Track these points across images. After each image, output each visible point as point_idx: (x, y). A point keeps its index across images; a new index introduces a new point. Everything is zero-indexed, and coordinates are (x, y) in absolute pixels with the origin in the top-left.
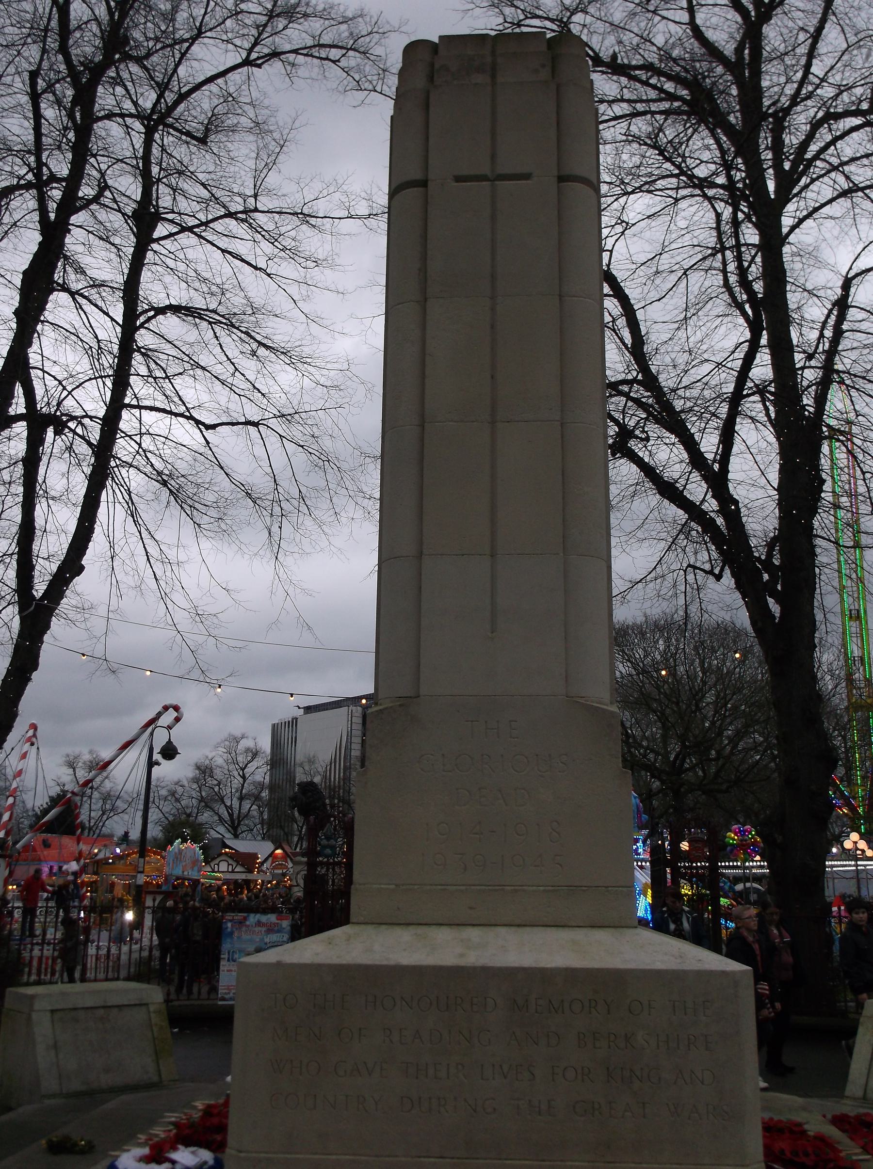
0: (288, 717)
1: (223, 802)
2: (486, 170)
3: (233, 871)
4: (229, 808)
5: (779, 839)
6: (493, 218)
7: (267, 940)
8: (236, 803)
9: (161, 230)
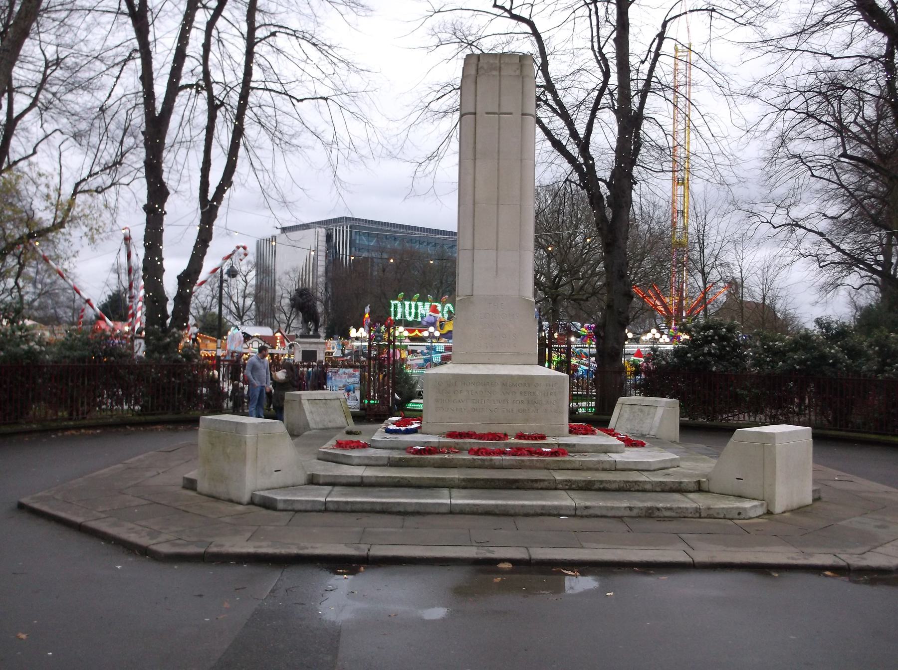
0: (268, 235)
1: (231, 298)
2: (497, 111)
5: (602, 334)
6: (499, 129)
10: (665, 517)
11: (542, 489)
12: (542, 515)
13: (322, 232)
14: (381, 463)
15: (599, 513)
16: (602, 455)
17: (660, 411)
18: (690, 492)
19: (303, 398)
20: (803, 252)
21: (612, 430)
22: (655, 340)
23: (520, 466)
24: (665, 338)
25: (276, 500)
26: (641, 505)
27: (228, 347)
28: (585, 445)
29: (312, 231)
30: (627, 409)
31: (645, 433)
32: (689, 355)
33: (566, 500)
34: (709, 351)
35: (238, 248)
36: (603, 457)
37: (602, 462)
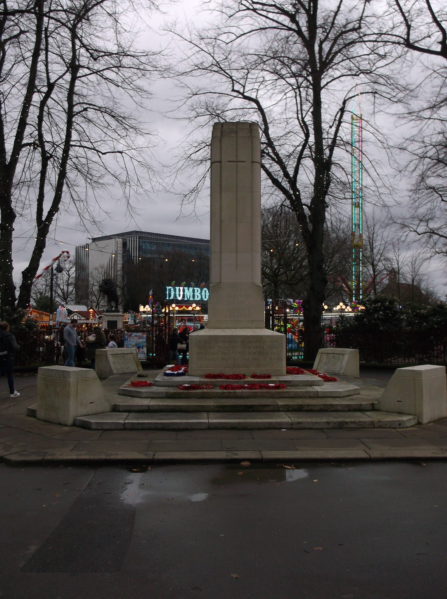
0: (83, 243)
2: (235, 160)
3: (80, 319)
4: (62, 290)
5: (307, 307)
7: (139, 341)
8: (65, 288)
9: (81, 72)
10: (351, 428)
11: (269, 411)
12: (269, 428)
13: (120, 241)
14: (162, 396)
15: (307, 426)
16: (309, 387)
17: (346, 357)
18: (367, 411)
19: (108, 353)
20: (437, 250)
21: (315, 371)
22: (342, 310)
23: (254, 396)
24: (349, 309)
25: (90, 423)
26: (335, 420)
27: (57, 319)
28: (297, 381)
29: (113, 240)
30: (325, 356)
31: (336, 372)
32: (365, 320)
33: (285, 418)
34: (378, 317)
35: (63, 252)
36: (309, 389)
37: (309, 392)
